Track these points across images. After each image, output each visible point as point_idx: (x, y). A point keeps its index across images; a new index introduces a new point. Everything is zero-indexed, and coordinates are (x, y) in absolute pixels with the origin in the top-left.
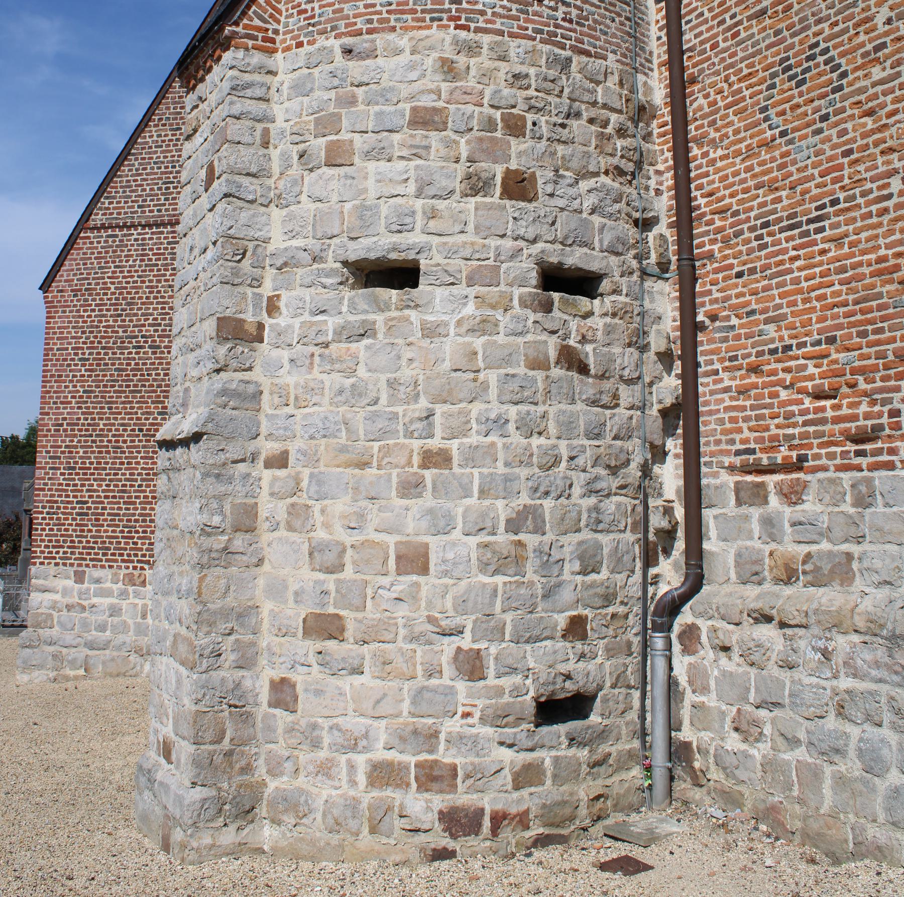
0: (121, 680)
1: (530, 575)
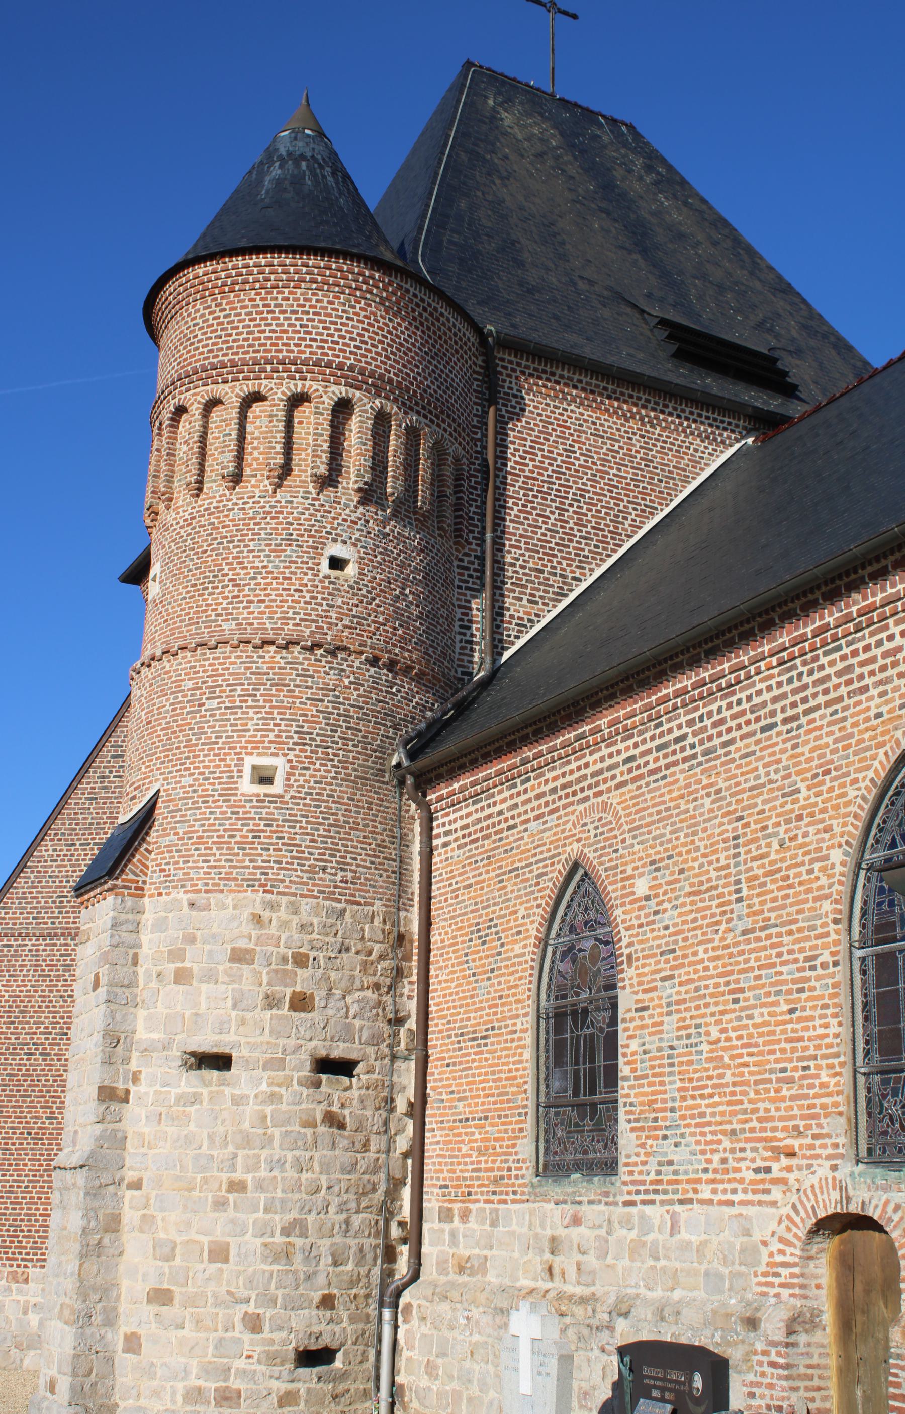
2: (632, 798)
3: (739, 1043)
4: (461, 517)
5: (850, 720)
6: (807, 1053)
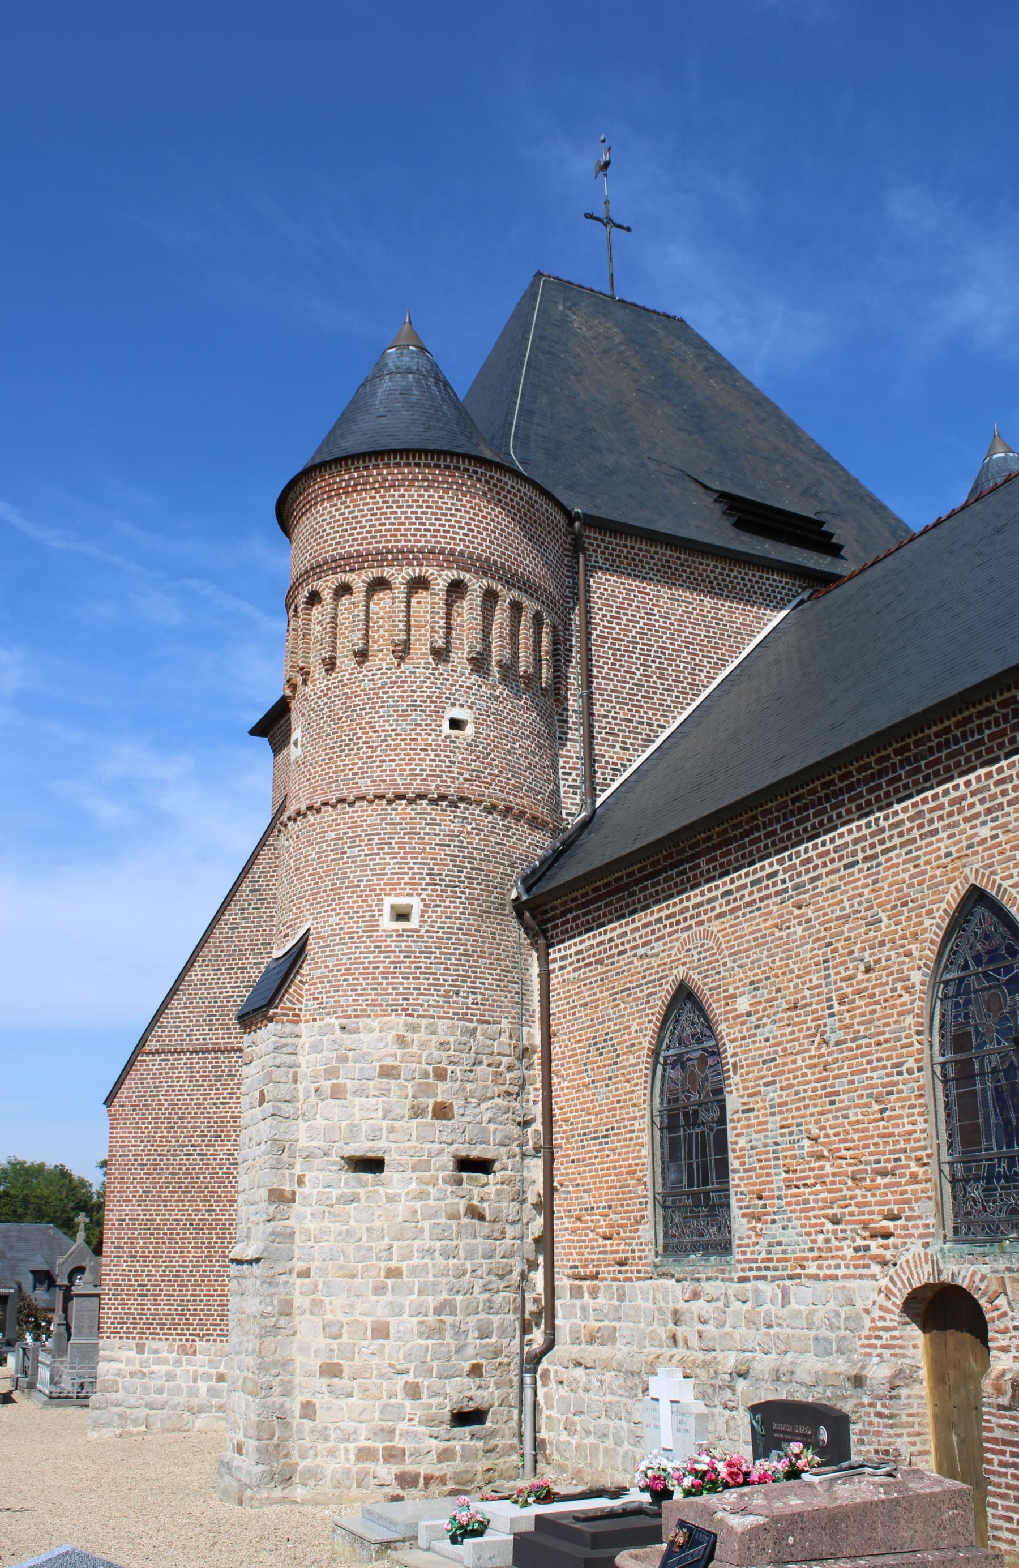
0: (177, 1434)
1: (448, 1339)
2: (731, 926)
3: (837, 1139)
4: (559, 677)
5: (923, 859)
6: (898, 1147)
